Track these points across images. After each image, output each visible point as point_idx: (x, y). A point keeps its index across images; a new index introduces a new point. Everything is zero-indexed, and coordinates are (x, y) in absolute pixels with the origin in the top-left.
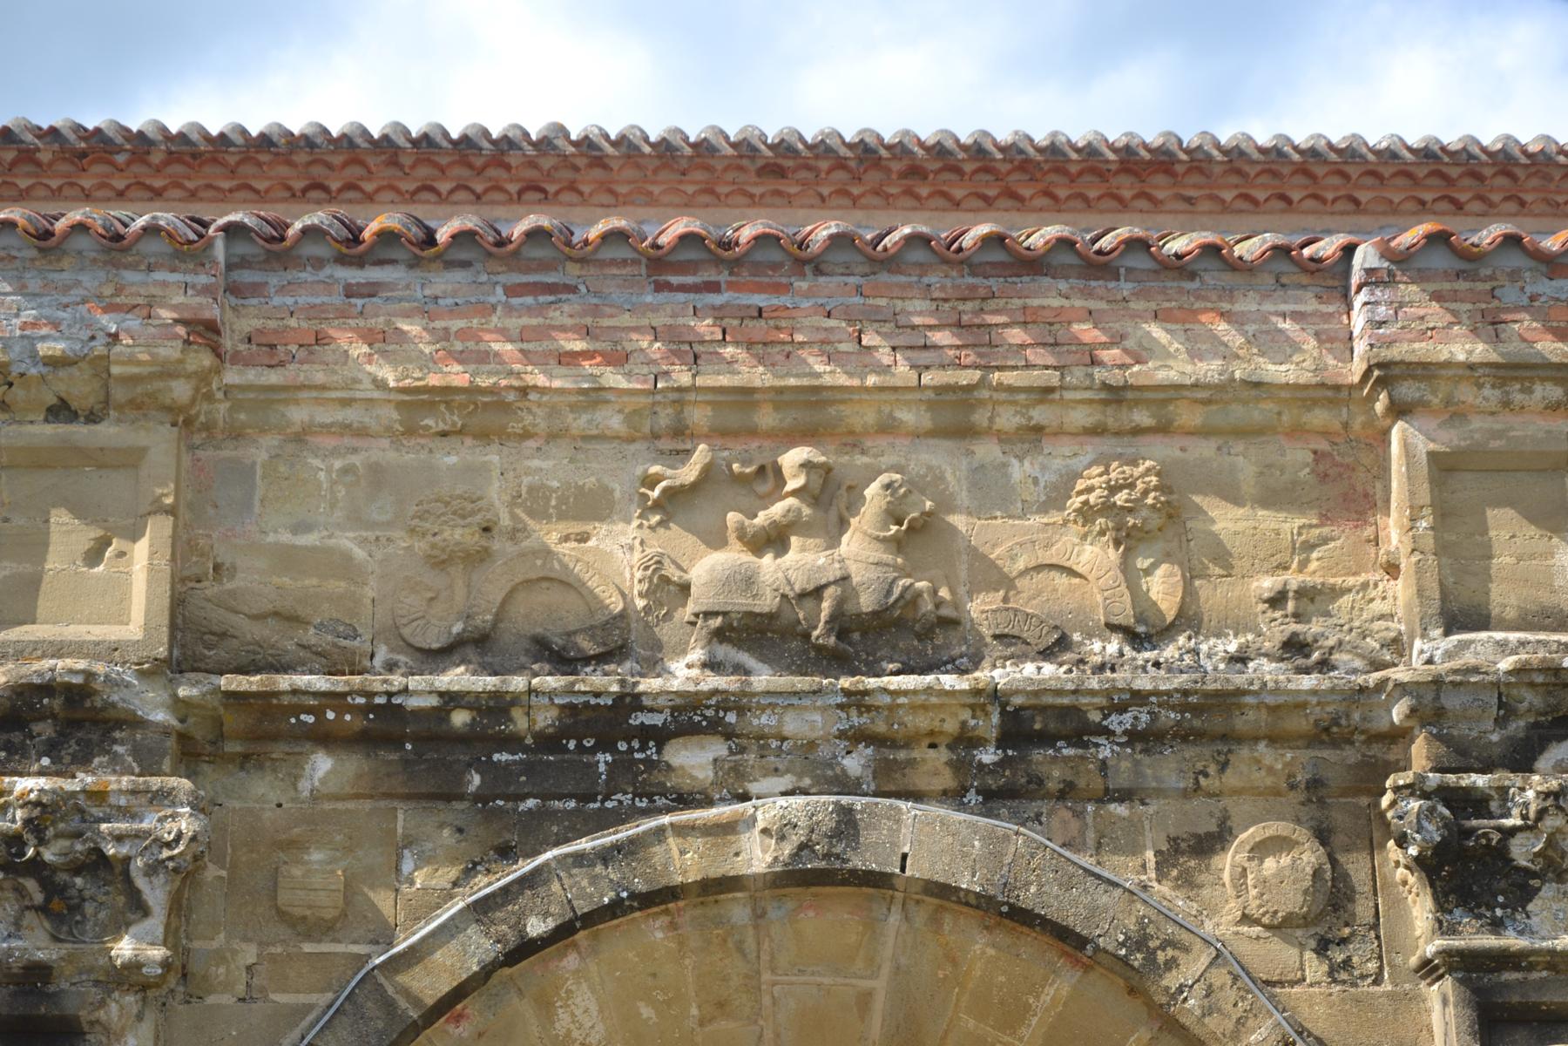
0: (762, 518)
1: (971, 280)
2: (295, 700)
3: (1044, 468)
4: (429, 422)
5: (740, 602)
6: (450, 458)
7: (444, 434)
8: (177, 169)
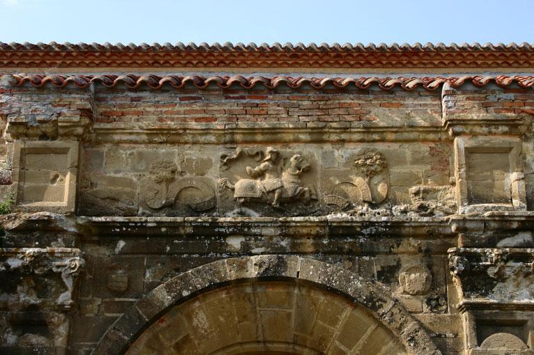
0: (257, 169)
1: (322, 95)
2: (113, 224)
3: (345, 152)
4: (156, 139)
5: (250, 194)
6: (163, 150)
7: (161, 143)
8: (115, 57)
